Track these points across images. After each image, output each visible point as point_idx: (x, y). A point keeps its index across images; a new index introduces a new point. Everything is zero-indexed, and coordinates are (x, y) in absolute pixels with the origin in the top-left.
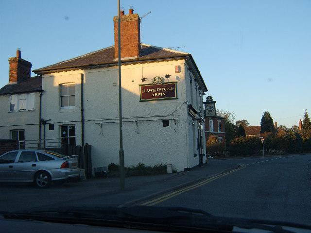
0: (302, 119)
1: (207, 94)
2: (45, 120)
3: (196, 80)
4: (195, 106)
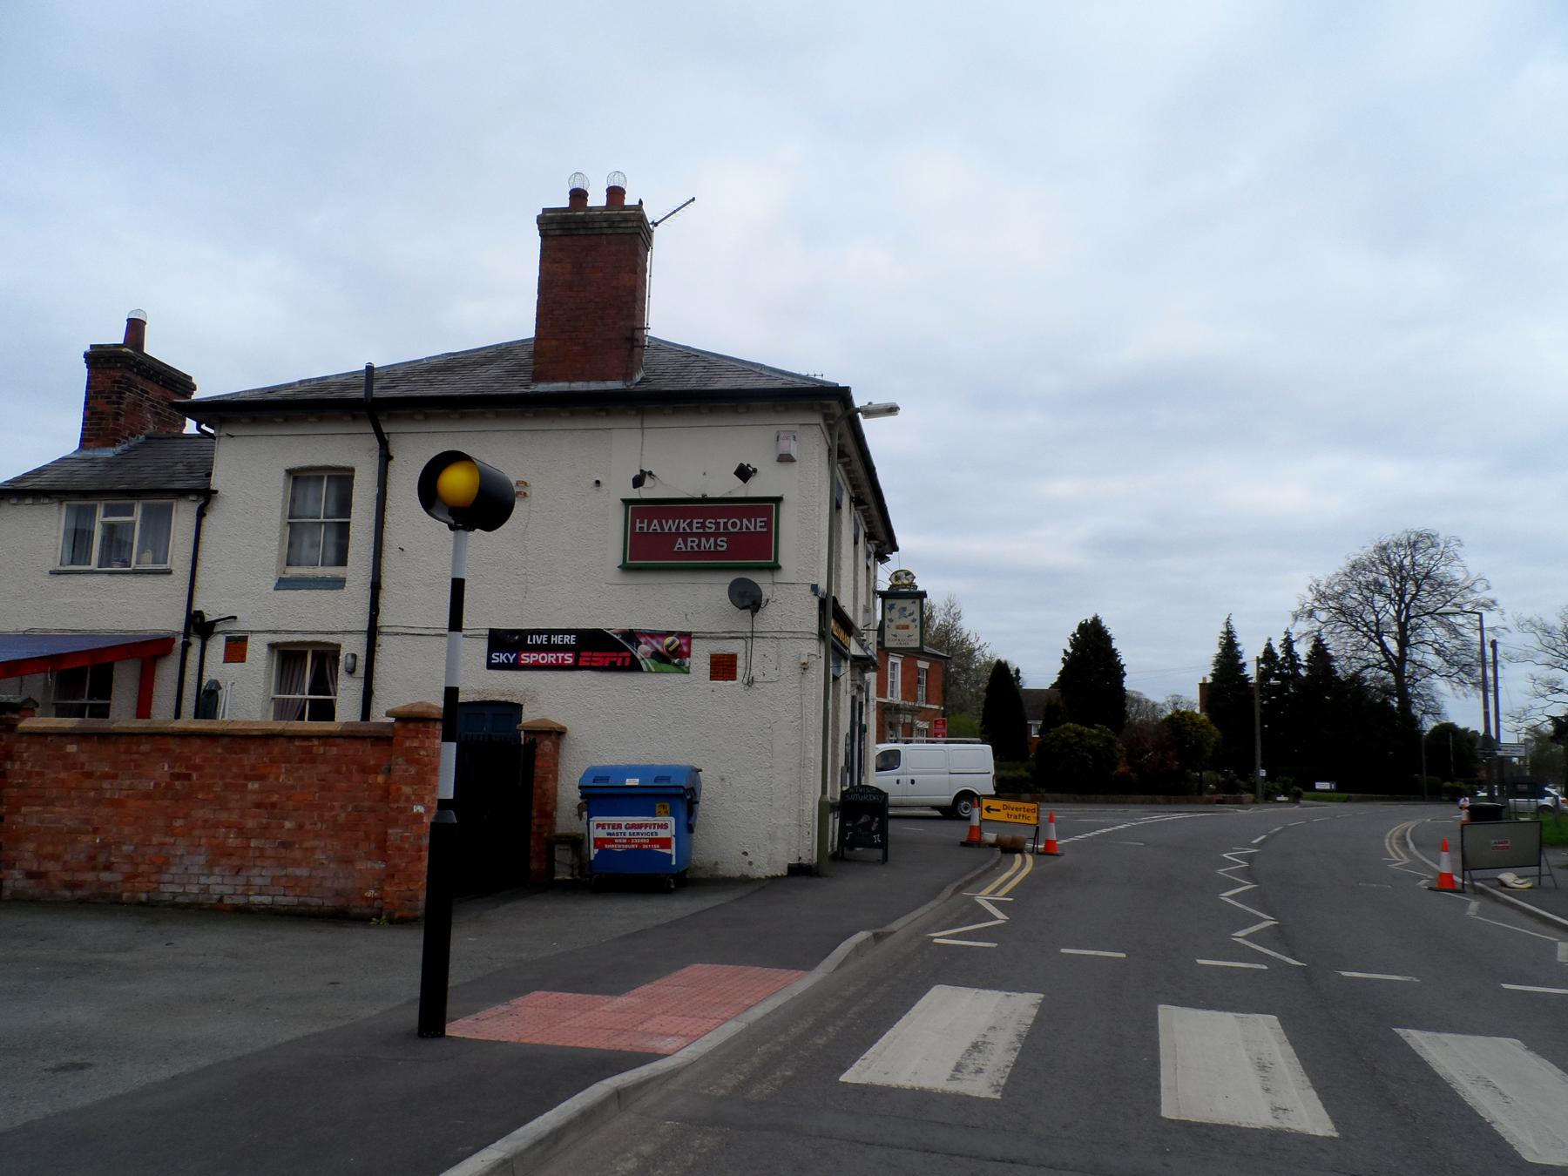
0: (1206, 672)
1: (895, 562)
2: (208, 618)
3: (857, 501)
4: (846, 603)
